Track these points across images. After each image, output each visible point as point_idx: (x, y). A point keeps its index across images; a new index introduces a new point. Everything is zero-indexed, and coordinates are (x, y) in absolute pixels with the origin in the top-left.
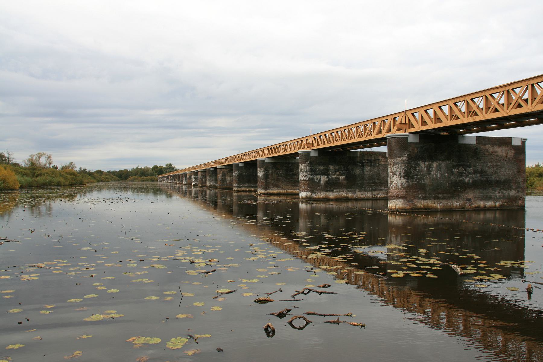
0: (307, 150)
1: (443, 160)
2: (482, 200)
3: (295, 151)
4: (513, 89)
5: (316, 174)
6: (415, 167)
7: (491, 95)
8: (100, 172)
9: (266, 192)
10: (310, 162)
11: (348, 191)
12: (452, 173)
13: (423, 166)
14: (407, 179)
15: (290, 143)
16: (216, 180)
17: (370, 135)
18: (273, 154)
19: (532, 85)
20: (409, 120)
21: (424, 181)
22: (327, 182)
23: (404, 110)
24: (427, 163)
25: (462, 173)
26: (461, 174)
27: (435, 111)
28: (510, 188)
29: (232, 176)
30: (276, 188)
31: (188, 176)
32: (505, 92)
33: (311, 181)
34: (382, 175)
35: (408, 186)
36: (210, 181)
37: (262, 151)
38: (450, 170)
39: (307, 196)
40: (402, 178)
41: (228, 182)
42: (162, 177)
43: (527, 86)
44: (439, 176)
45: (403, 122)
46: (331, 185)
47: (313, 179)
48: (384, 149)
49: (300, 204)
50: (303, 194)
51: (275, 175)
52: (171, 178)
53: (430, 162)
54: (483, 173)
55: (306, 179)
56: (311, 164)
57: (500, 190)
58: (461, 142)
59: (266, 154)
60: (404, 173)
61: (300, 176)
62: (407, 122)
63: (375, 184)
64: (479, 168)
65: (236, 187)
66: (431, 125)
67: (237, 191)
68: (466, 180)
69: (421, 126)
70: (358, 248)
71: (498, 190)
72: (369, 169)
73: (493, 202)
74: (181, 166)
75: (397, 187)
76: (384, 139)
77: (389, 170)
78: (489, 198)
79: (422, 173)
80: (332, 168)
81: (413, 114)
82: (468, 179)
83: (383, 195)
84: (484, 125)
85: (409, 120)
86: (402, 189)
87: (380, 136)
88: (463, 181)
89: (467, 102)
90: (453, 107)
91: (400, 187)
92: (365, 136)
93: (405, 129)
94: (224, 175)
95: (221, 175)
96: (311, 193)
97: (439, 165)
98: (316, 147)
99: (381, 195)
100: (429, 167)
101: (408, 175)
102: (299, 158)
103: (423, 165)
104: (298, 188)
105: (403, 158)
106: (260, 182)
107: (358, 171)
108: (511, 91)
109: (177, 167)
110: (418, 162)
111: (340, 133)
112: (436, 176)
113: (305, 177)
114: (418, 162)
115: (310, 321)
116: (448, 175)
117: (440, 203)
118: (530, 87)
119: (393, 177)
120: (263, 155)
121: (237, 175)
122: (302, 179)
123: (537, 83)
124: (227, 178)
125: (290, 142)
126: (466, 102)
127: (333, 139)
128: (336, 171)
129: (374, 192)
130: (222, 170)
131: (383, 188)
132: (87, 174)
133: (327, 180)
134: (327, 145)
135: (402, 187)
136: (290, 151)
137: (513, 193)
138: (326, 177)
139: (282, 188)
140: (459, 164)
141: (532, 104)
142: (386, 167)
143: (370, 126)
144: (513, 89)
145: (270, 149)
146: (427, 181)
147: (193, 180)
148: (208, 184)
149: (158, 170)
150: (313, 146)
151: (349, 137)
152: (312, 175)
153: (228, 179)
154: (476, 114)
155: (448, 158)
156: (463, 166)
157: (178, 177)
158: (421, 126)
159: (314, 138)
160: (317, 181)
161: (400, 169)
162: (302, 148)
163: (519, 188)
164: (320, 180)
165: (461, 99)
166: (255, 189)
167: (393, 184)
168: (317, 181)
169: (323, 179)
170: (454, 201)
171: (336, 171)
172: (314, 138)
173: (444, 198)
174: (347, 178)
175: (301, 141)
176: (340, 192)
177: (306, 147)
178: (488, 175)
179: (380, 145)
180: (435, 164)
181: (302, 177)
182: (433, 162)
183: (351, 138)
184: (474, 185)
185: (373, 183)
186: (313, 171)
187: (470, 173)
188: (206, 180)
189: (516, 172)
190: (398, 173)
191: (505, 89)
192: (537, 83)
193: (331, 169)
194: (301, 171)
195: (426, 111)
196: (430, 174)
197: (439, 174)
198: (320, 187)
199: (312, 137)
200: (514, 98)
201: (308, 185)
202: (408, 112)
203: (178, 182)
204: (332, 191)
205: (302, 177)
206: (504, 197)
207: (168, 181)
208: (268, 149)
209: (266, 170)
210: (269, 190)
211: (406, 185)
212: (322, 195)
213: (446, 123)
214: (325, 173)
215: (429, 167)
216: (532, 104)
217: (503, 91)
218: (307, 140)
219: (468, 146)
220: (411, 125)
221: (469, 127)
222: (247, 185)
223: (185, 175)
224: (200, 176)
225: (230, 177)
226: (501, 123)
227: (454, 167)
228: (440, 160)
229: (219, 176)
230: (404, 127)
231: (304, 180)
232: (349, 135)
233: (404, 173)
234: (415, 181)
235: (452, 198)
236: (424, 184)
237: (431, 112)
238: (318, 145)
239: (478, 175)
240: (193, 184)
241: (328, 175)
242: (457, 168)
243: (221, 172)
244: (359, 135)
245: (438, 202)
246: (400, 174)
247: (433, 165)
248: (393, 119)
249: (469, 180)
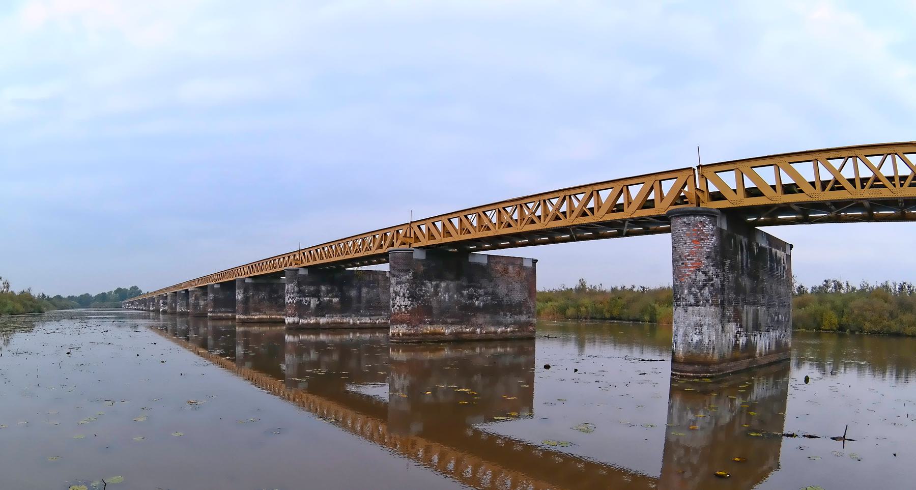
0: (294, 267)
1: (452, 280)
2: (493, 325)
3: (281, 269)
4: (526, 204)
5: (305, 296)
6: (421, 287)
7: (504, 208)
8: (59, 297)
10: (298, 282)
11: (342, 316)
12: (462, 295)
13: (429, 286)
15: (275, 260)
16: (188, 305)
17: (369, 250)
18: (254, 272)
19: (544, 201)
20: (415, 233)
21: (431, 303)
22: (317, 305)
23: (409, 222)
24: (434, 283)
26: (470, 297)
27: (444, 224)
28: (521, 313)
29: (207, 300)
30: (258, 313)
31: (156, 301)
32: (519, 206)
33: (299, 303)
34: (383, 297)
35: (413, 309)
36: (181, 306)
37: (242, 269)
38: (459, 290)
39: (294, 322)
40: (406, 300)
41: (201, 307)
42: (126, 303)
43: (540, 201)
44: (447, 298)
45: (408, 235)
46: (322, 310)
47: (301, 301)
48: (385, 267)
49: (286, 337)
50: (289, 320)
51: (256, 298)
52: (137, 303)
53: (438, 282)
54: (494, 295)
55: (293, 302)
56: (299, 284)
57: (511, 315)
58: (471, 260)
59: (246, 273)
60: (408, 294)
61: (286, 298)
62: (412, 235)
63: (374, 308)
64: (490, 290)
65: (211, 312)
66: (440, 240)
67: (213, 319)
68: (477, 303)
69: (429, 240)
70: (378, 385)
71: (509, 314)
72: (367, 290)
73: (504, 328)
74: (148, 287)
75: (400, 310)
76: (386, 255)
77: (391, 290)
78: (499, 324)
79: (428, 294)
80: (323, 288)
81: (419, 227)
82: (478, 302)
83: (383, 321)
84: (496, 242)
85: (415, 233)
86: (406, 312)
89: (479, 215)
90: (482, 215)
91: (404, 310)
92: (363, 252)
93: (410, 243)
94: (197, 299)
95: (193, 298)
96: (299, 318)
97: (448, 285)
98: (306, 264)
99: (379, 321)
100: (437, 287)
101: (413, 297)
102: (284, 278)
103: (429, 285)
104: (283, 313)
105: (408, 277)
106: (239, 306)
107: (353, 293)
108: (523, 205)
109: (144, 291)
110: (425, 282)
111: (334, 247)
112: (445, 298)
113: (292, 299)
114: (425, 282)
116: (457, 297)
117: (449, 328)
118: (542, 202)
119: (396, 298)
120: (243, 274)
121: (212, 298)
122: (289, 302)
123: (549, 200)
124: (200, 302)
125: (274, 259)
126: (477, 214)
127: (325, 254)
128: (328, 292)
129: (372, 318)
130: (195, 292)
131: (383, 313)
132: (51, 303)
133: (318, 302)
134: (319, 262)
135: (406, 310)
136: (275, 268)
137: (524, 318)
138: (316, 299)
139: (265, 314)
140: (469, 285)
142: (386, 288)
143: (369, 239)
144: (526, 204)
145: (250, 267)
146: (434, 304)
147: (162, 305)
148: (178, 310)
149: (122, 294)
150: (302, 262)
151: (344, 252)
152: (300, 296)
153: (202, 303)
154: (488, 229)
155: (457, 278)
156: (474, 287)
157: (144, 302)
158: (429, 240)
159: (304, 253)
160: (306, 304)
161: (404, 289)
162: (288, 265)
163: (530, 313)
164: (310, 303)
165: (473, 211)
166: (233, 314)
167: (396, 307)
168: (306, 304)
169: (314, 302)
170: (463, 327)
171: (328, 292)
172: (304, 253)
173: (452, 323)
174: (342, 301)
175: (287, 258)
176: (333, 317)
177: (293, 264)
178: (499, 298)
179: (380, 262)
180: (443, 284)
181: (289, 299)
183: (347, 253)
184: (486, 309)
185: (372, 307)
186: (301, 293)
187: (480, 296)
188: (176, 306)
189: (527, 296)
190: (401, 294)
191: (519, 203)
192: (549, 200)
193: (322, 291)
194: (287, 292)
195: (433, 223)
196: (438, 295)
197: (447, 295)
198: (310, 311)
199: (301, 252)
200: (527, 213)
201: (296, 309)
202: (414, 224)
203: (144, 308)
204: (324, 316)
205: (289, 299)
206: (515, 323)
207: (134, 308)
208: (249, 267)
209: (246, 291)
210: (249, 315)
211: (410, 308)
213: (456, 237)
214: (316, 294)
215: (437, 287)
217: (516, 205)
218: (294, 256)
219: (479, 266)
220: (417, 239)
221: (479, 243)
222: (223, 309)
223: (152, 299)
224: (169, 299)
225: (204, 300)
226: (514, 240)
227: (464, 288)
228: (448, 280)
229: (192, 300)
230: (409, 240)
231: (290, 302)
232: (345, 249)
233: (408, 294)
234: (420, 304)
235: (460, 323)
236: (431, 307)
237: (439, 225)
238: (308, 261)
239: (489, 298)
240: (161, 310)
241: (319, 297)
242: (467, 289)
243: (194, 295)
244: (357, 249)
245: (446, 327)
246: (404, 294)
247: (441, 285)
248: (396, 231)
249: (480, 303)
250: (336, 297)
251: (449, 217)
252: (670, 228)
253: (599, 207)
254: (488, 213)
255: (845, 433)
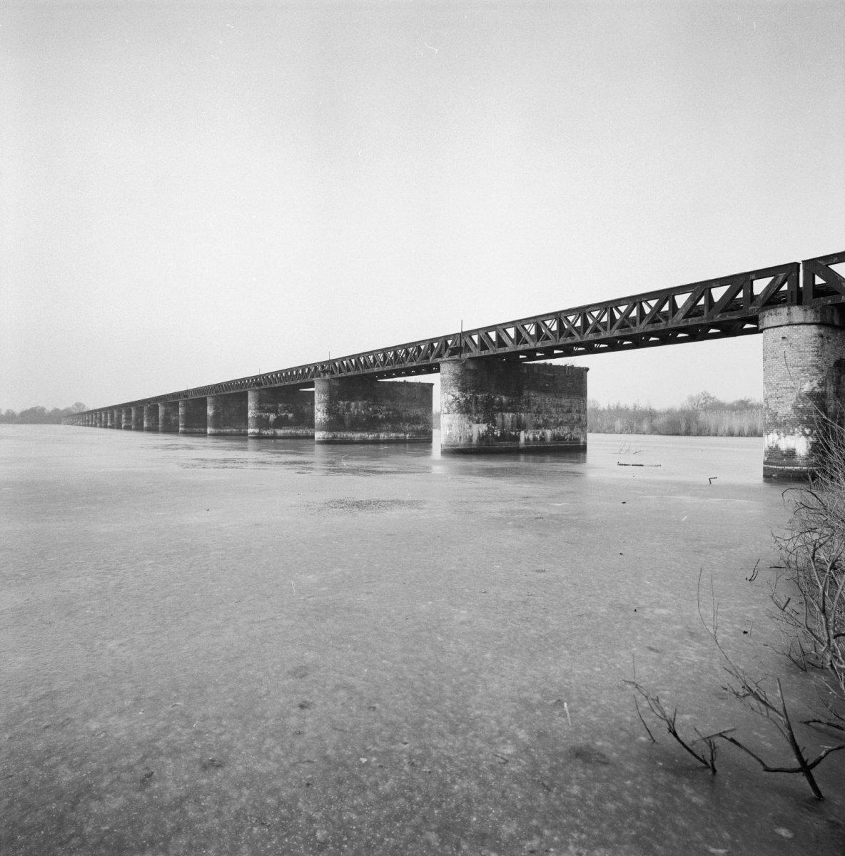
9: (218, 430)
14: (329, 415)
22: (275, 419)
25: (376, 411)
26: (375, 412)
28: (418, 423)
40: (325, 414)
46: (280, 423)
47: (261, 416)
61: (249, 414)
87: (425, 363)
88: (377, 417)
115: (803, 725)
128: (286, 408)
134: (278, 385)
139: (235, 427)
141: (611, 329)
164: (269, 417)
169: (272, 417)
174: (296, 416)
182: (351, 402)
184: (388, 419)
206: (413, 431)
212: (270, 432)
213: (510, 348)
214: (275, 411)
216: (611, 329)
225: (175, 416)
238: (341, 372)
241: (276, 413)
250: (290, 412)
251: (505, 327)
252: (757, 328)
253: (674, 313)
254: (527, 327)
255: (57, 417)
